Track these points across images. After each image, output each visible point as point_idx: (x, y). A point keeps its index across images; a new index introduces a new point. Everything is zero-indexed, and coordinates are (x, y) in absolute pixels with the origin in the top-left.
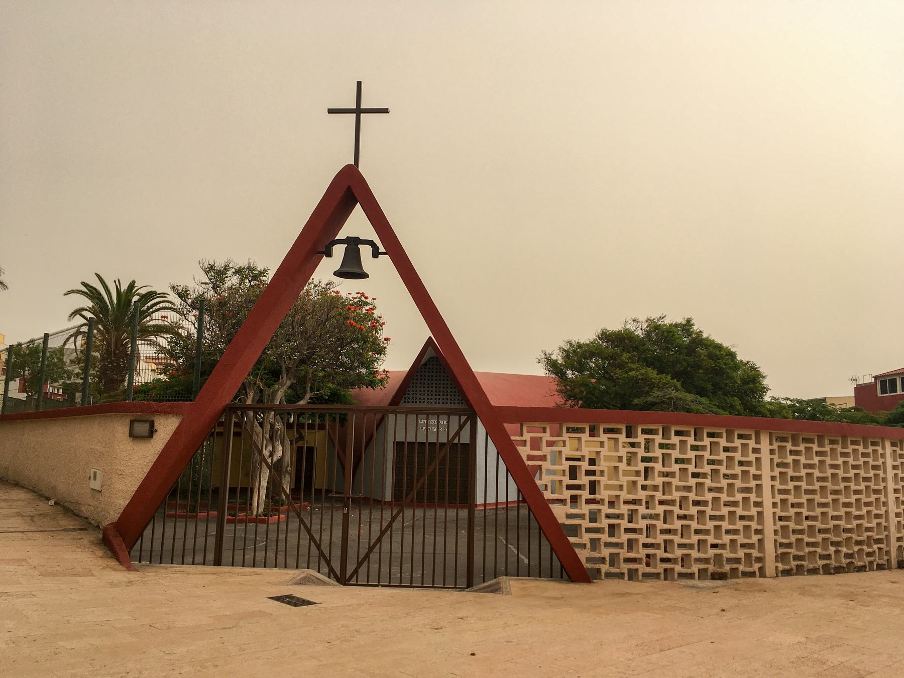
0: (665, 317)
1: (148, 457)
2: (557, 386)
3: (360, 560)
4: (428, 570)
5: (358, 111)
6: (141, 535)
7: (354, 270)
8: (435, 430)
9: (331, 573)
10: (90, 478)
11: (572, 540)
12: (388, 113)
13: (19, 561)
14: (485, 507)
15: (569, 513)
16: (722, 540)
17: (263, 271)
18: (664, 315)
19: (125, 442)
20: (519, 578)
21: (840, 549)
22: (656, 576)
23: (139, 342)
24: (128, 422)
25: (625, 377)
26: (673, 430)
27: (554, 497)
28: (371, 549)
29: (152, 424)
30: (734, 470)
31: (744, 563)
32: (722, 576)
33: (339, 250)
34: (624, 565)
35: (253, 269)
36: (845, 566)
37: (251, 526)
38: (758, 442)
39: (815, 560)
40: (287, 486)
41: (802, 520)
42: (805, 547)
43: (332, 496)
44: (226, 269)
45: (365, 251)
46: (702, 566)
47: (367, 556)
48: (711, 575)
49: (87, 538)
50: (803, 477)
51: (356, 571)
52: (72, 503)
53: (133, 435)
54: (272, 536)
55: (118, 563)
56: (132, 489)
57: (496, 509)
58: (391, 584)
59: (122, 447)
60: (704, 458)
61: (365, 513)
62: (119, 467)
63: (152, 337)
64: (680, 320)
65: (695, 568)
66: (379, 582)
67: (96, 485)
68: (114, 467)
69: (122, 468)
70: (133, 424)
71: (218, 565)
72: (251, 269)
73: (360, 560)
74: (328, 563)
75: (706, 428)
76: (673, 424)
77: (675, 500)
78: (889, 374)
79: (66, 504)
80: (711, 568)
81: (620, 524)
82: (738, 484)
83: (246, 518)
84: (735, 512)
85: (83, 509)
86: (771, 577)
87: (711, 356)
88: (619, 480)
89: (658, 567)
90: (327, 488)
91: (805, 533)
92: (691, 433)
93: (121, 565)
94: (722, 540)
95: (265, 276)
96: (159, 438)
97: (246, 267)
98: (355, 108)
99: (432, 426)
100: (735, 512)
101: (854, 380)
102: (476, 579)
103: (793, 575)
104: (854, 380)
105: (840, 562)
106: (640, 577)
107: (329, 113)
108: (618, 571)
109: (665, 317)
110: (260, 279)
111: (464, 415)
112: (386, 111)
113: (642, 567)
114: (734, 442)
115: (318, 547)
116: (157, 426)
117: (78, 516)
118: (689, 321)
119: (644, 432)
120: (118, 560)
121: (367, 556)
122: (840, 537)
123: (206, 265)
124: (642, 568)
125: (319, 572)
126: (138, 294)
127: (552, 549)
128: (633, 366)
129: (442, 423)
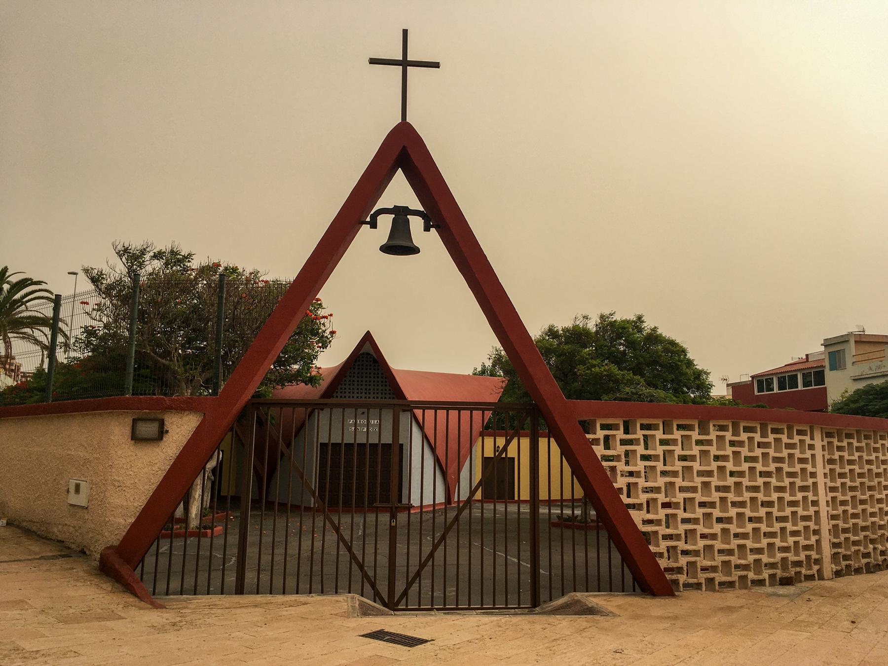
0: (614, 313)
1: (156, 464)
2: (501, 383)
3: (410, 580)
4: (464, 585)
5: (405, 63)
6: (142, 560)
7: (398, 242)
8: (365, 430)
9: (377, 597)
10: (68, 491)
11: (652, 548)
12: (439, 67)
13: (19, 604)
14: (421, 510)
15: (646, 519)
16: (787, 542)
17: (188, 255)
18: (613, 312)
19: (124, 446)
20: (612, 593)
21: (876, 546)
22: (731, 584)
23: (10, 335)
24: (129, 421)
25: (587, 373)
26: (742, 424)
27: (630, 501)
28: (422, 566)
29: (162, 423)
30: (795, 467)
31: (806, 566)
32: (786, 582)
33: (386, 222)
34: (701, 575)
35: (177, 254)
36: (881, 563)
37: (192, 540)
38: (812, 438)
39: (858, 558)
40: (208, 493)
41: (848, 518)
42: (851, 546)
43: (376, 505)
44: (143, 252)
45: (416, 224)
46: (771, 571)
47: (418, 574)
48: (780, 581)
49: (80, 569)
50: (713, 471)
51: (405, 593)
52: (34, 522)
53: (136, 438)
54: (204, 553)
55: (136, 599)
56: (135, 505)
57: (421, 512)
58: (422, 607)
59: (120, 453)
60: (769, 455)
61: (281, 523)
62: (115, 477)
63: (28, 330)
64: (632, 317)
65: (766, 574)
66: (432, 606)
67: (81, 500)
68: (110, 477)
69: (121, 479)
70: (136, 423)
71: (241, 594)
72: (173, 253)
73: (410, 580)
74: (373, 586)
75: (770, 424)
76: (741, 420)
77: (746, 501)
78: (762, 374)
79: (24, 524)
80: (779, 573)
81: (696, 529)
82: (715, 481)
83: (199, 532)
84: (797, 512)
85: (55, 530)
86: (828, 580)
87: (666, 350)
88: (693, 481)
89: (733, 575)
90: (232, 495)
91: (850, 531)
92: (757, 429)
93: (142, 600)
94: (787, 542)
95: (189, 261)
96: (171, 439)
97: (169, 250)
98: (408, 60)
99: (361, 425)
100: (797, 512)
101: (724, 380)
102: (544, 595)
103: (843, 576)
104: (724, 380)
105: (877, 560)
106: (717, 587)
107: (370, 63)
108: (695, 581)
109: (614, 313)
110: (184, 265)
111: (489, 410)
112: (436, 65)
113: (718, 576)
114: (793, 439)
115: (361, 567)
116: (168, 425)
117: (46, 538)
118: (640, 318)
119: (643, 427)
120: (134, 593)
121: (418, 574)
122: (876, 535)
123: (120, 247)
124: (719, 577)
125: (362, 596)
126: (8, 283)
127: (623, 560)
128: (595, 362)
129: (373, 423)
